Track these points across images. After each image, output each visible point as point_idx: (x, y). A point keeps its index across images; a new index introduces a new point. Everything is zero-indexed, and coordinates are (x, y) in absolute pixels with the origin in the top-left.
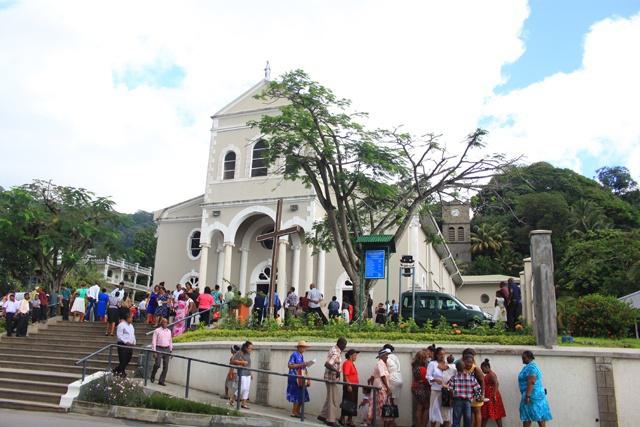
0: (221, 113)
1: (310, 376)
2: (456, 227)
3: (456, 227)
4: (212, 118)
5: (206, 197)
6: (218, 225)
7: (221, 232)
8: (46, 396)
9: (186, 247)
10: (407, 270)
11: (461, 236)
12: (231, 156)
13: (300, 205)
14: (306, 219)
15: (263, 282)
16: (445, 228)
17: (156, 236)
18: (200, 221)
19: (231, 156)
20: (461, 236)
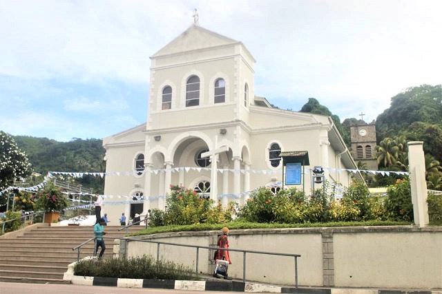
0: (158, 55)
1: (229, 248)
2: (364, 146)
3: (364, 146)
4: (150, 58)
5: (148, 125)
6: (159, 148)
7: (162, 155)
8: (440, 131)
9: (250, 149)
10: (319, 178)
11: (369, 153)
12: (167, 90)
13: (227, 129)
14: (233, 141)
15: (135, 202)
16: (354, 147)
17: (105, 159)
18: (144, 145)
19: (167, 90)
20: (369, 153)
